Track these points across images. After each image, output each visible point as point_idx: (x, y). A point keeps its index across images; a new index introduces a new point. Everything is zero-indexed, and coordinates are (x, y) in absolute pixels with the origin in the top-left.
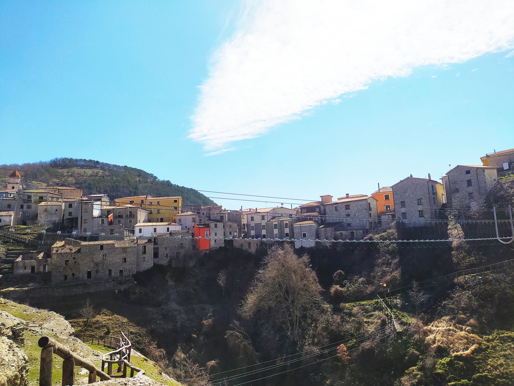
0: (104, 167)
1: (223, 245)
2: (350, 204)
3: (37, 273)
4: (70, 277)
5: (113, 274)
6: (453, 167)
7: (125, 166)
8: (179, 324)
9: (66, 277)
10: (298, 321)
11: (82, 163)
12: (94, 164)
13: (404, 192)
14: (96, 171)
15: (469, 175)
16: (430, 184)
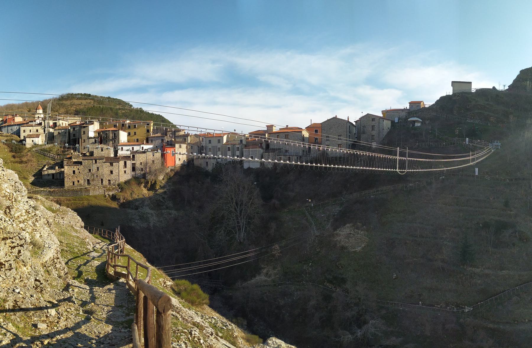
2: (290, 134)
3: (56, 179)
5: (104, 182)
7: (109, 97)
8: (151, 225)
9: (74, 182)
10: (244, 227)
11: (80, 96)
12: (87, 96)
13: (330, 129)
14: (89, 101)
15: (374, 122)
16: (348, 124)
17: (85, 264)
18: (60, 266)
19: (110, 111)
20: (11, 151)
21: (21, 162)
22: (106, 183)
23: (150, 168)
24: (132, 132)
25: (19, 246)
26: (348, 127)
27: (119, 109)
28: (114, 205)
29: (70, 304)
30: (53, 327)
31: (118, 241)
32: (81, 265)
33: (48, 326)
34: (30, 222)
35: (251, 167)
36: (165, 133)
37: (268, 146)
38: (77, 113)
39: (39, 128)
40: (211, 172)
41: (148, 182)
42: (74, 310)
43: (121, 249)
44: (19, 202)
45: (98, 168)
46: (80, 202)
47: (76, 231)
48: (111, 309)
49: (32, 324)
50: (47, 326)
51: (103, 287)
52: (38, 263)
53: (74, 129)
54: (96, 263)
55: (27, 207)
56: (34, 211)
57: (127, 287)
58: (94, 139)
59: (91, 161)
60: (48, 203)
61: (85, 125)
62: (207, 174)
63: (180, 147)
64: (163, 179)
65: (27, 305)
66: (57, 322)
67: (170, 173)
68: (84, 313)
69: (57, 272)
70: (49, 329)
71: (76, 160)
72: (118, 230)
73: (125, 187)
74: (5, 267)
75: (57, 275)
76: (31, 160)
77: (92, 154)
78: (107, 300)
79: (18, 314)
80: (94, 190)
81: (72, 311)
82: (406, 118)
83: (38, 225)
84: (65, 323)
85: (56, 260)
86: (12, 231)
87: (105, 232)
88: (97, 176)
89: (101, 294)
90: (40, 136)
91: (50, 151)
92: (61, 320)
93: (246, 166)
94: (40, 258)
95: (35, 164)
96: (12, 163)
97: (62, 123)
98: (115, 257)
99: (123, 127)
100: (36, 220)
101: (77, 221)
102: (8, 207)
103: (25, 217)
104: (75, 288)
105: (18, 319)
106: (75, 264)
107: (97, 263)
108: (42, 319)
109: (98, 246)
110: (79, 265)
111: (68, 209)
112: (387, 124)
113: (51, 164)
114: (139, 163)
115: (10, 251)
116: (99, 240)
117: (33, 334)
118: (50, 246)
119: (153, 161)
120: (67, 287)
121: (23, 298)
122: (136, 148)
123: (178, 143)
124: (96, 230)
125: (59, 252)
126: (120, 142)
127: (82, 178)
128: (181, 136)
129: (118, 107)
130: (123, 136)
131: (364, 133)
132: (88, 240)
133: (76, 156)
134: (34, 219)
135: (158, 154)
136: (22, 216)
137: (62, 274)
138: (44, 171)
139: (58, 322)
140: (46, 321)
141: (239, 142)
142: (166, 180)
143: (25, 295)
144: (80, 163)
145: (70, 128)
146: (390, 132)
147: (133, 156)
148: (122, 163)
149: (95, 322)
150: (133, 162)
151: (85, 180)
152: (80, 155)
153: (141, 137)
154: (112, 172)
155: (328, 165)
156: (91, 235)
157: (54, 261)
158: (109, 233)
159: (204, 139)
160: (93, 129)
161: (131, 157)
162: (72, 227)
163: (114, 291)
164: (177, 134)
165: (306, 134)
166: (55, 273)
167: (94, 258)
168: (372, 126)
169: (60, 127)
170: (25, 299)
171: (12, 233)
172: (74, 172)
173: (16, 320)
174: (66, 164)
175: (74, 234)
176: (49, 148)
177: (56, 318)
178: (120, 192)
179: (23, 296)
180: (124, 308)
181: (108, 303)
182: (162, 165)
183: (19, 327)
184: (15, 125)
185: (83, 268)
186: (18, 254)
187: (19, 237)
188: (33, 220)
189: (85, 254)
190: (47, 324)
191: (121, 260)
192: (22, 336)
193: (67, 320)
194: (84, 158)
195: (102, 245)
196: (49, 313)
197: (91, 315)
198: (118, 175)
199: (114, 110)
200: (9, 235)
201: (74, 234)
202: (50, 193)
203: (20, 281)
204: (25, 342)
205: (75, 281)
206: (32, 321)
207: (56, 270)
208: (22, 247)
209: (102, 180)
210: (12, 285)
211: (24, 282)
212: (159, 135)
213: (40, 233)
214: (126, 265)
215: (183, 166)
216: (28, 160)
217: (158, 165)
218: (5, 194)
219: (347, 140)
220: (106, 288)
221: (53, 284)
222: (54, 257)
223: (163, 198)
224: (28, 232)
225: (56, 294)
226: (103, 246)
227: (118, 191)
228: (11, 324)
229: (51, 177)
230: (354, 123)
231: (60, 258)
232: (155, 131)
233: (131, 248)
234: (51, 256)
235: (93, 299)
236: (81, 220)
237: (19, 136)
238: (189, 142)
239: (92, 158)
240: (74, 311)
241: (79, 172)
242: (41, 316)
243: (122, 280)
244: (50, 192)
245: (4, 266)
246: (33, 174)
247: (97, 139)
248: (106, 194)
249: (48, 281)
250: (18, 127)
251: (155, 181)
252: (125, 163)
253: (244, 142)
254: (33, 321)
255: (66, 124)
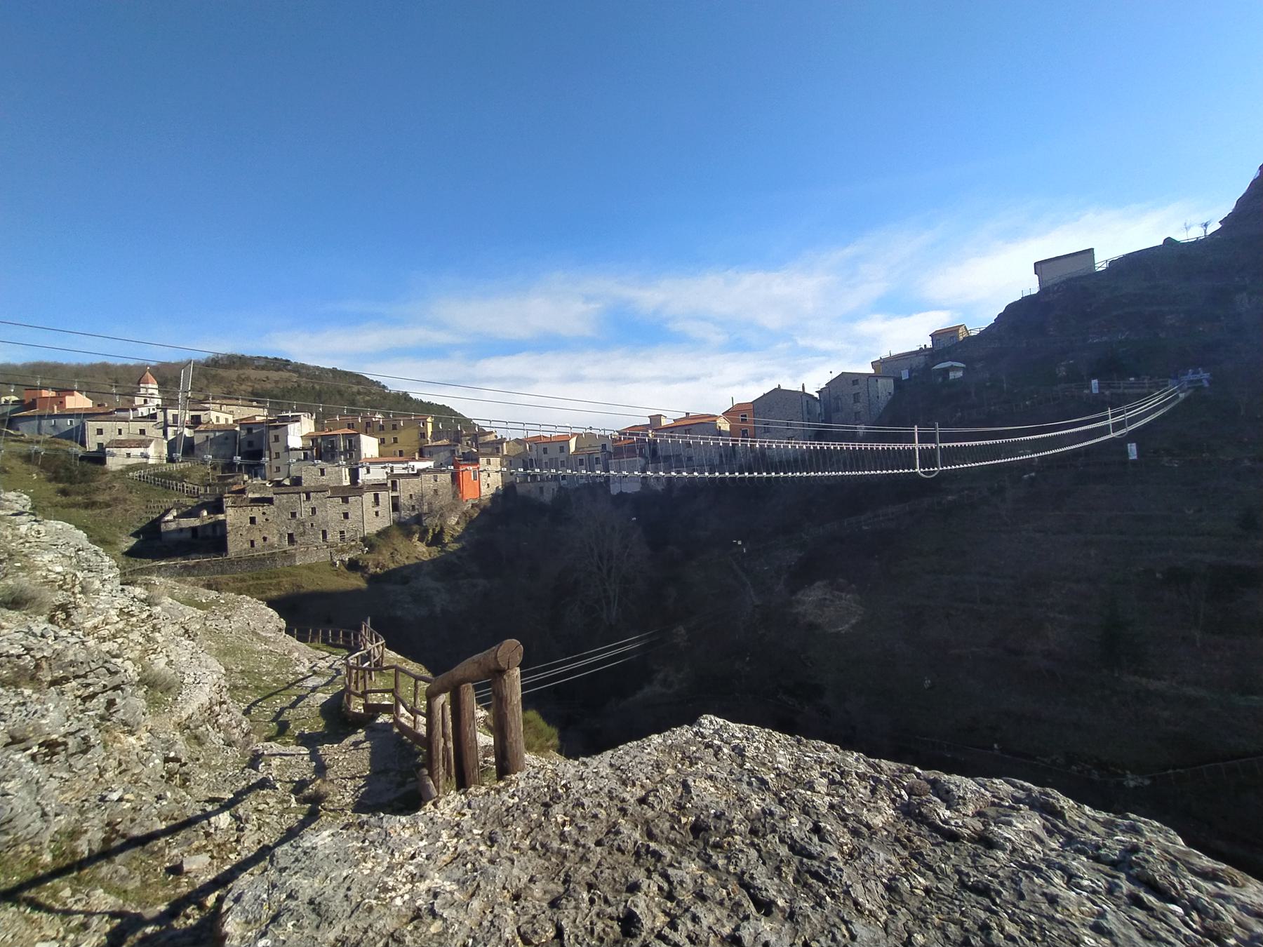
0: (299, 369)
1: (929, 345)
4: (259, 543)
5: (329, 537)
6: (835, 375)
8: (438, 609)
9: (252, 542)
10: (617, 598)
11: (262, 363)
12: (281, 365)
17: (293, 706)
18: (228, 719)
19: (338, 397)
20: (56, 478)
21: (91, 505)
22: (333, 537)
23: (430, 504)
24: (389, 438)
25: (110, 689)
26: (805, 404)
27: (359, 393)
28: (356, 582)
29: (265, 792)
30: (225, 857)
31: (369, 645)
32: (283, 710)
33: (212, 857)
34: (136, 636)
35: (624, 491)
36: (457, 439)
37: (654, 453)
38: (256, 397)
39: (148, 426)
40: (550, 504)
41: (426, 531)
42: (276, 802)
43: (377, 661)
44: (97, 592)
45: (314, 510)
46: (270, 581)
47: (266, 640)
48: (363, 783)
49: (167, 869)
50: (210, 857)
51: (339, 741)
52: (167, 726)
53: (250, 430)
54: (321, 697)
55: (121, 601)
56: (148, 608)
57: (396, 730)
58: (302, 452)
59: (297, 495)
60: (185, 589)
61: (277, 423)
62: (541, 508)
63: (489, 463)
64: (458, 523)
65: (148, 823)
66: (235, 841)
67: (472, 511)
68: (302, 803)
69: (222, 735)
70: (215, 864)
71: (257, 495)
72: (366, 627)
73: (379, 542)
74: (66, 750)
75: (222, 742)
76: (125, 500)
77: (297, 481)
78: (352, 765)
79: (119, 858)
80: (305, 553)
81: (270, 808)
82: (927, 369)
83: (160, 639)
84: (255, 837)
85: (217, 708)
86: (82, 656)
87: (336, 635)
88: (312, 525)
89: (336, 757)
90: (152, 445)
91: (183, 477)
92: (246, 831)
93: (615, 489)
94: (171, 711)
95: (136, 507)
96: (60, 508)
97: (218, 418)
98: (363, 677)
99: (369, 428)
100: (155, 628)
101: (273, 620)
102: (63, 607)
103: (117, 625)
104: (272, 758)
105: (124, 871)
106: (268, 710)
107: (321, 698)
108: (196, 844)
109: (322, 664)
110: (278, 709)
111: (241, 596)
112: (885, 387)
113: (186, 506)
114: (408, 495)
115: (81, 708)
116: (324, 653)
117: (173, 892)
118: (198, 680)
119: (436, 491)
120: (255, 760)
121: (133, 809)
122: (399, 469)
123: (484, 455)
124: (315, 633)
125: (224, 689)
126: (363, 457)
127: (275, 532)
128: (488, 443)
129: (355, 388)
130: (369, 446)
131: (838, 410)
132: (296, 655)
133: (255, 486)
134: (148, 626)
135: (445, 478)
136: (106, 625)
137: (236, 734)
138: (168, 521)
139: (238, 841)
140: (205, 846)
141: (600, 448)
142: (463, 525)
143: (138, 801)
144: (270, 501)
145: (238, 429)
146: (894, 401)
147: (394, 483)
148: (368, 497)
149: (329, 816)
150: (394, 494)
151: (281, 534)
152: (267, 485)
153: (409, 448)
154: (346, 516)
155: (756, 474)
156: (303, 645)
157: (211, 712)
158: (346, 635)
159: (534, 446)
160: (299, 432)
161: (389, 485)
162: (254, 633)
163: (367, 744)
164: (481, 440)
165: (725, 426)
166: (216, 738)
167: (314, 689)
168: (854, 395)
169: (211, 427)
170: (140, 809)
171: (82, 663)
172: (253, 520)
173: (114, 875)
174: (230, 504)
175: (261, 647)
176: (181, 471)
177: (231, 832)
178: (367, 552)
179: (134, 805)
180: (392, 774)
181: (354, 772)
182: (454, 497)
183: (125, 891)
184: (70, 416)
185: (288, 715)
186: (107, 709)
187: (108, 670)
188: (146, 628)
189: (290, 685)
190: (209, 854)
191: (377, 681)
192: (139, 911)
193: (259, 829)
194: (277, 490)
195: (328, 660)
196: (213, 825)
197: (319, 803)
198: (361, 519)
199: (346, 394)
200: (72, 669)
201: (261, 647)
202: (187, 570)
203: (120, 773)
204: (155, 921)
205: (272, 744)
206: (166, 859)
207: (220, 730)
208: (119, 691)
209: (324, 533)
210: (94, 788)
211: (130, 774)
212: (445, 442)
213: (168, 656)
214: (393, 687)
215: (495, 497)
216: (115, 499)
217: (446, 498)
218: (47, 578)
219: (803, 426)
220: (348, 743)
221: (213, 762)
222: (210, 703)
223: (459, 558)
224: (129, 659)
225: (225, 781)
226: (335, 661)
227: (363, 551)
228: (100, 891)
229: (189, 535)
230: (817, 395)
231: (228, 701)
232: (437, 434)
233: (399, 656)
234: (203, 701)
235: (321, 769)
236: (276, 615)
237: (83, 443)
238: (505, 453)
239: (297, 489)
240: (275, 805)
241: (267, 520)
242: (192, 840)
243: (383, 719)
244: (185, 567)
245: (63, 747)
246: (133, 530)
247: (309, 452)
248: (336, 559)
249: (198, 759)
250: (76, 422)
251: (442, 529)
252: (376, 496)
253: (610, 448)
254: (169, 861)
255: (227, 420)
